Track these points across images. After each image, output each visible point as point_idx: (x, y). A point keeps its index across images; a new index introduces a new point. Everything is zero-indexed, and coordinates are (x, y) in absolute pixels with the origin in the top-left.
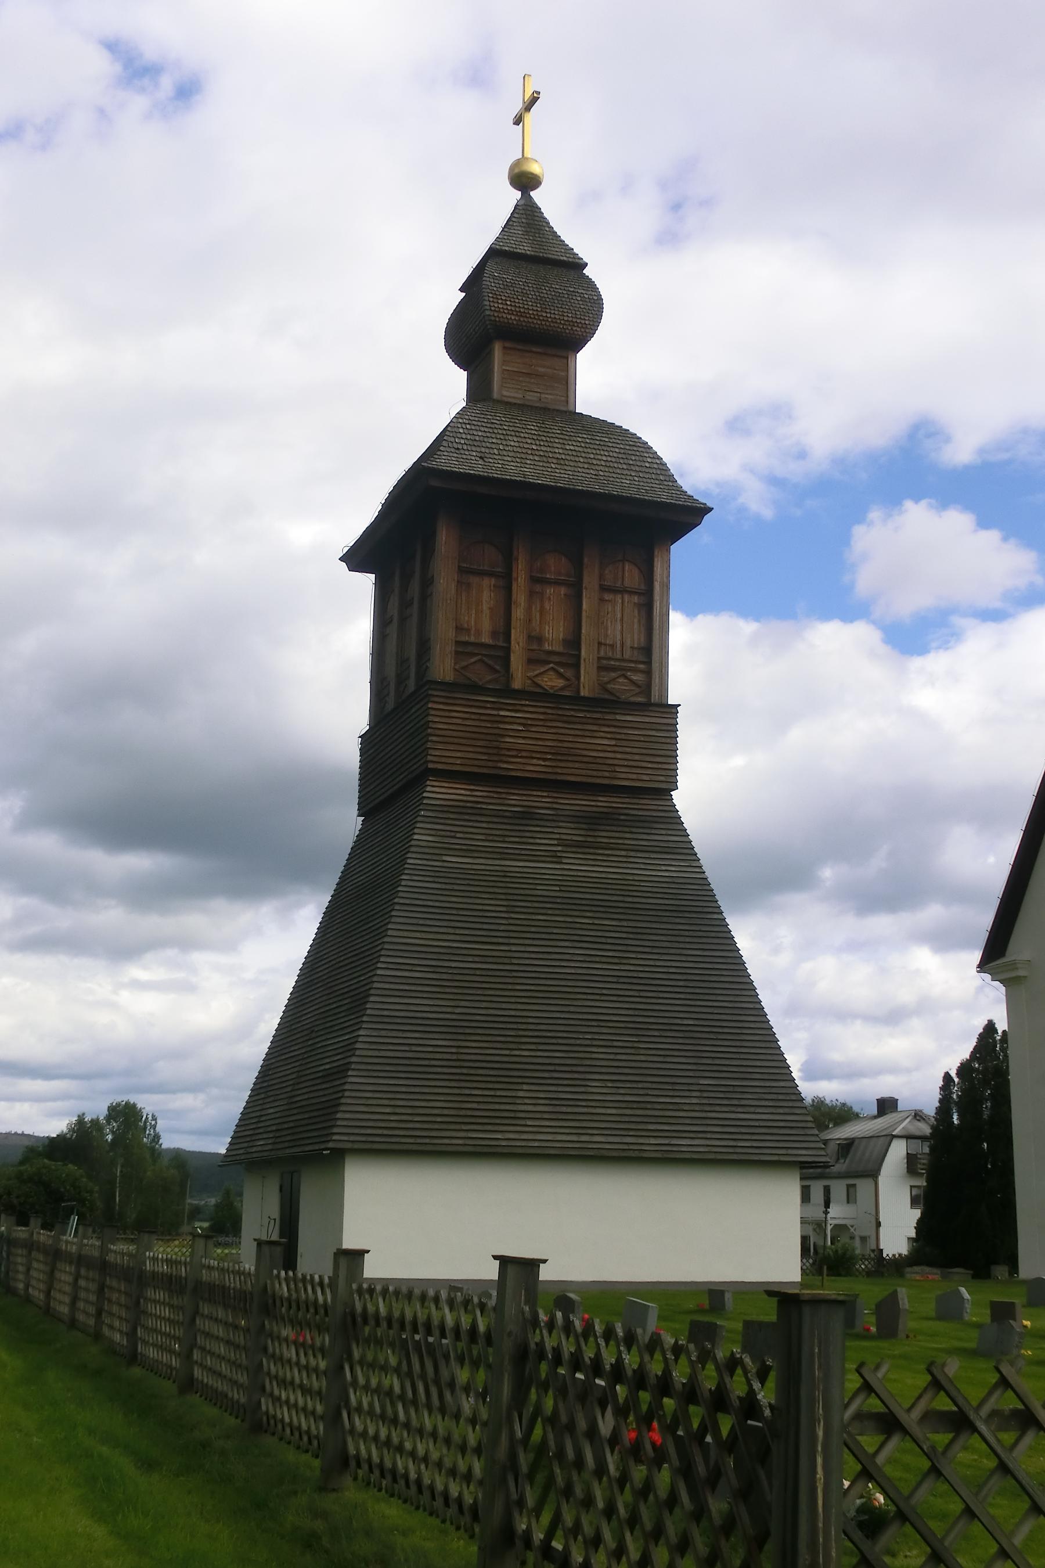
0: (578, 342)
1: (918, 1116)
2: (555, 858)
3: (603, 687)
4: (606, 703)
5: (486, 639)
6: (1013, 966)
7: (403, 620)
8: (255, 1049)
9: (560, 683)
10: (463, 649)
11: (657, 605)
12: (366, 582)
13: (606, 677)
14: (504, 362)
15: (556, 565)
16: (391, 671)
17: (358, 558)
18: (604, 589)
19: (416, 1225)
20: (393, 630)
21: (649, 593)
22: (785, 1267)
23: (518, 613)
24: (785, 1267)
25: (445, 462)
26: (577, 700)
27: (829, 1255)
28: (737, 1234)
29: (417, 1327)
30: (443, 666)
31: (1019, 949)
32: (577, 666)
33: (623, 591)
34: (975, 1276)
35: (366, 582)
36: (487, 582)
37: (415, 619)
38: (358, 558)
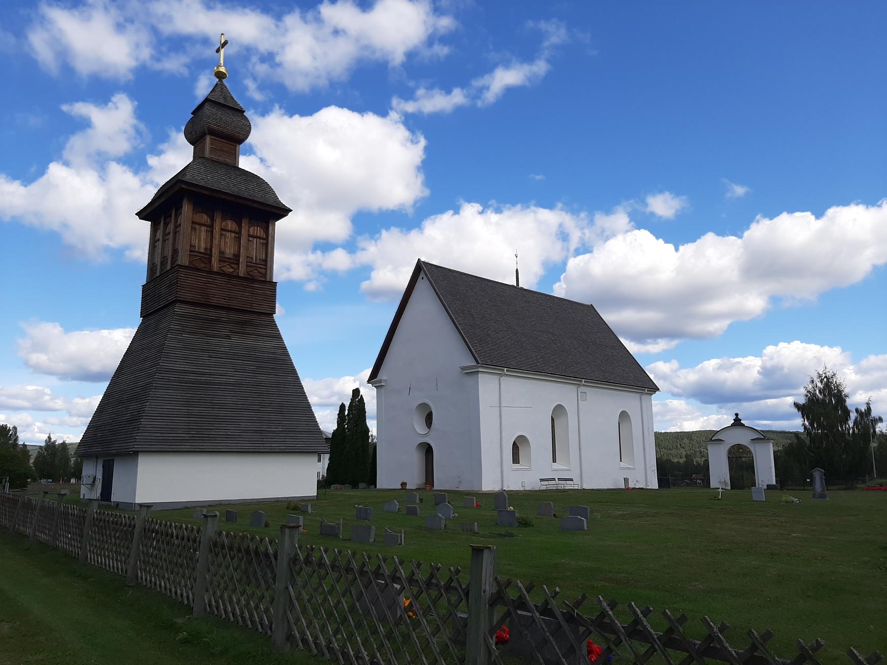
2: (229, 337)
3: (248, 272)
4: (249, 279)
5: (202, 250)
6: (380, 381)
8: (114, 363)
10: (222, 259)
11: (270, 245)
12: (148, 224)
13: (250, 269)
15: (230, 225)
17: (143, 214)
18: (249, 236)
19: (162, 481)
20: (159, 244)
21: (267, 239)
23: (216, 242)
26: (238, 277)
28: (297, 478)
30: (183, 259)
31: (382, 375)
32: (238, 264)
33: (257, 237)
35: (148, 224)
37: (171, 241)
38: (143, 214)
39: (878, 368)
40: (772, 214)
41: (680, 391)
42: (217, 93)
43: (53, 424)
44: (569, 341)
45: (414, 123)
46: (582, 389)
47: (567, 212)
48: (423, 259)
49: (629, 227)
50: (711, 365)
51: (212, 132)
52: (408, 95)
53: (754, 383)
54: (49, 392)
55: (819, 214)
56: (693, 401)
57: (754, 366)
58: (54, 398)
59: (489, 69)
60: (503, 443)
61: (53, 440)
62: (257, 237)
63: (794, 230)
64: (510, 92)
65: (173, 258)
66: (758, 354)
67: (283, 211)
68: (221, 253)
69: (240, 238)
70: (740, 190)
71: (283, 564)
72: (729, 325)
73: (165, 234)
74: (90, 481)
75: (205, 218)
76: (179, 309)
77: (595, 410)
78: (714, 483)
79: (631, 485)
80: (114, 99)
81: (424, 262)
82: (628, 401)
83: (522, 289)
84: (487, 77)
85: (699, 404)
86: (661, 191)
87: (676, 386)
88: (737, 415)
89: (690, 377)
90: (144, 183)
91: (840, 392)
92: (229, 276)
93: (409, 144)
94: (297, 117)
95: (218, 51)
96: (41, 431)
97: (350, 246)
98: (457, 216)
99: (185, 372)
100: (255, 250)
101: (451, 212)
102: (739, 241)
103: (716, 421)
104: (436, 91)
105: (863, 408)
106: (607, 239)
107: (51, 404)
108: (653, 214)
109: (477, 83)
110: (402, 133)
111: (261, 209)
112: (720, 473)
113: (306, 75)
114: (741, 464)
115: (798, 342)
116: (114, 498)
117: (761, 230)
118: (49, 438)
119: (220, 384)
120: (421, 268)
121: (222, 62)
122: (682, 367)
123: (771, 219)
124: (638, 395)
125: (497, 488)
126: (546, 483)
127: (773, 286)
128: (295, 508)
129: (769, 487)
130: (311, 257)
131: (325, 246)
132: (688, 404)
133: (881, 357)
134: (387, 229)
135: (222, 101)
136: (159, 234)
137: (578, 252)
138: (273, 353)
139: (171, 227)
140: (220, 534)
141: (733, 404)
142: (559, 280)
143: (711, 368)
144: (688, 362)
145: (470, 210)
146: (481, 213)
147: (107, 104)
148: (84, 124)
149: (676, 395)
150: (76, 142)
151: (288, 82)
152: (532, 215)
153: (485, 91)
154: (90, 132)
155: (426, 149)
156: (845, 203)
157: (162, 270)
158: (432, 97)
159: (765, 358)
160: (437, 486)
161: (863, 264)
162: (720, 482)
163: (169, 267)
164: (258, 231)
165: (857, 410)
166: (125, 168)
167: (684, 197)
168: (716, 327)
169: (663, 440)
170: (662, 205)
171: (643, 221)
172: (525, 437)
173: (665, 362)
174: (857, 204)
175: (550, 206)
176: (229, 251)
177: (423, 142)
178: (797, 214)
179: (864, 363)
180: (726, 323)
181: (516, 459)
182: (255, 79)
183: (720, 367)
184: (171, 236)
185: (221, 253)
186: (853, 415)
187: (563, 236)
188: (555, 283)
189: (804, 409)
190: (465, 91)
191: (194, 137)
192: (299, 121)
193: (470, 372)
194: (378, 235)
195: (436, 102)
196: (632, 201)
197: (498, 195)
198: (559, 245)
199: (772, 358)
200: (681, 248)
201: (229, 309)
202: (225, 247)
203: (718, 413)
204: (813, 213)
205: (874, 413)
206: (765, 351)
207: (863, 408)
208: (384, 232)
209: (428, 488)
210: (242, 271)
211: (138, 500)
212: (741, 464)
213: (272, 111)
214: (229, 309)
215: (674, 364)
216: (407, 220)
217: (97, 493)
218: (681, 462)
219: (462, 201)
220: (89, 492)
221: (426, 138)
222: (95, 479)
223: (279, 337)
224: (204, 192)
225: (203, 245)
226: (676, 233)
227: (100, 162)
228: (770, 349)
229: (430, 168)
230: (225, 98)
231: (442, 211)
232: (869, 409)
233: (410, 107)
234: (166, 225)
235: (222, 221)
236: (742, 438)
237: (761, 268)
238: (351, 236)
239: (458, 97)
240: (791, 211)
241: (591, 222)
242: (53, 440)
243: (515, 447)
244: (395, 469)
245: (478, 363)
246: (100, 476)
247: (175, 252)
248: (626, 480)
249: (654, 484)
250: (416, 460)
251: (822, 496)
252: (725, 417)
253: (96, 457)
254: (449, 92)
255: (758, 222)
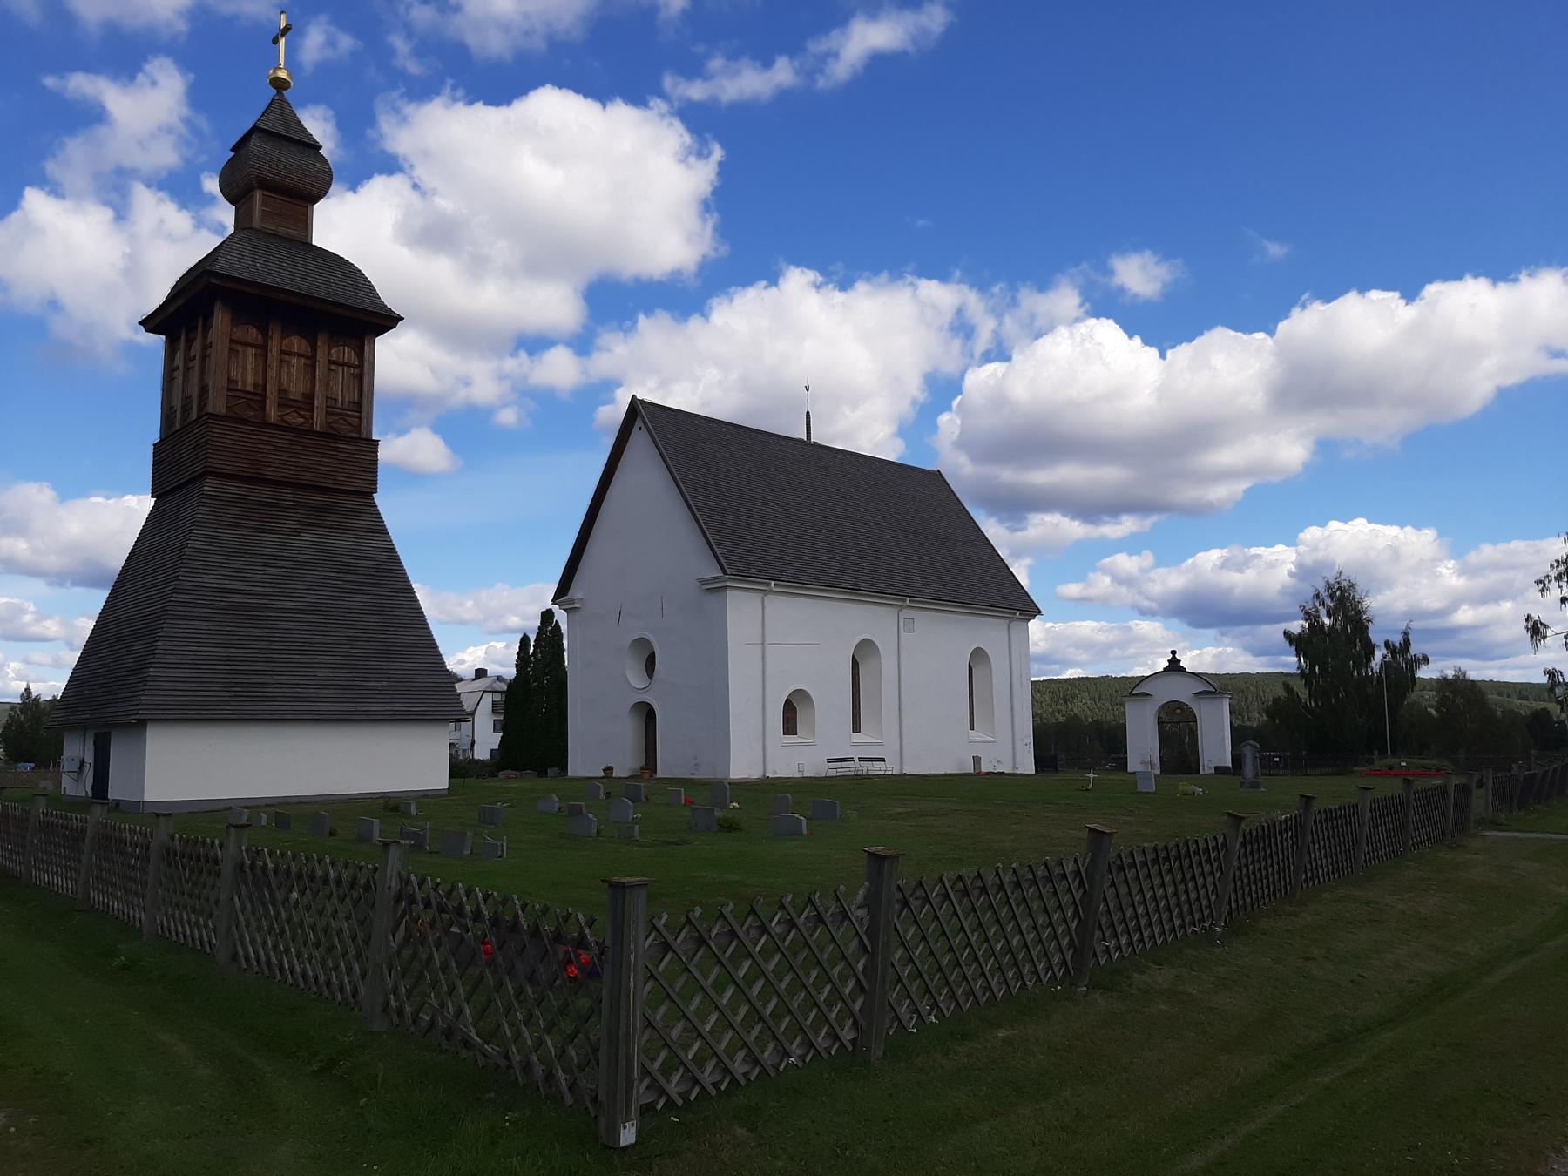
0: (316, 199)
1: (499, 679)
2: (296, 533)
4: (331, 435)
5: (249, 388)
6: (572, 601)
7: (187, 370)
9: (301, 420)
10: (284, 401)
13: (331, 418)
14: (264, 204)
15: (297, 344)
16: (177, 404)
17: (151, 323)
18: (330, 362)
19: (185, 767)
20: (179, 375)
21: (361, 367)
22: (439, 779)
23: (272, 373)
24: (439, 779)
25: (220, 266)
27: (461, 767)
29: (202, 834)
31: (576, 591)
33: (343, 364)
34: (539, 775)
36: (251, 351)
37: (197, 368)
38: (151, 323)
39: (1496, 567)
40: (1329, 295)
41: (1154, 605)
42: (274, 116)
43: (40, 665)
44: (887, 532)
45: (701, 122)
46: (906, 613)
47: (972, 286)
48: (639, 397)
49: (1080, 312)
50: (1210, 558)
51: (264, 185)
52: (693, 69)
53: (1284, 591)
54: (32, 608)
55: (1410, 294)
56: (1175, 622)
57: (1283, 562)
58: (40, 617)
59: (838, 19)
60: (768, 704)
61: (34, 695)
62: (343, 364)
63: (1365, 323)
64: (878, 62)
65: (200, 396)
66: (1291, 542)
67: (387, 320)
68: (282, 392)
69: (314, 367)
70: (1276, 250)
71: (227, 869)
72: (1245, 492)
73: (188, 359)
74: (75, 766)
75: (253, 334)
76: (209, 486)
77: (927, 648)
78: (1133, 765)
79: (984, 770)
80: (147, 67)
81: (642, 401)
82: (987, 632)
83: (816, 445)
84: (835, 33)
85: (1185, 628)
86: (1137, 248)
87: (1148, 598)
88: (1173, 653)
89: (1173, 580)
90: (199, 224)
91: (1359, 613)
92: (296, 430)
93: (692, 159)
94: (479, 106)
95: (276, 41)
96: (20, 677)
97: (582, 344)
98: (774, 290)
99: (221, 591)
100: (340, 386)
101: (763, 283)
102: (1270, 342)
103: (1215, 656)
104: (746, 61)
105: (1397, 640)
106: (1038, 336)
107: (36, 630)
108: (1122, 290)
109: (816, 46)
110: (675, 136)
111: (351, 315)
112: (1143, 746)
113: (505, 27)
114: (1177, 729)
115: (1363, 521)
116: (113, 794)
117: (1308, 322)
118: (28, 690)
119: (282, 610)
120: (636, 408)
121: (282, 60)
122: (1159, 563)
123: (1329, 301)
124: (1005, 623)
125: (756, 774)
126: (838, 765)
127: (1322, 422)
128: (396, 809)
129: (1220, 770)
130: (510, 364)
131: (534, 344)
132: (1167, 628)
133: (1502, 547)
134: (649, 312)
135: (280, 130)
136: (179, 356)
137: (987, 358)
138: (374, 559)
139: (197, 347)
140: (173, 838)
141: (1245, 628)
142: (949, 408)
143: (1209, 566)
144: (1170, 553)
145: (797, 281)
146: (818, 287)
147: (132, 78)
148: (92, 116)
149: (1145, 613)
150: (75, 148)
151: (472, 40)
152: (908, 292)
153: (830, 60)
154: (101, 131)
155: (723, 169)
156: (1455, 275)
157: (184, 419)
158: (737, 73)
159: (1301, 548)
160: (661, 772)
161: (1479, 385)
162: (1143, 763)
163: (194, 416)
164: (347, 354)
165: (1387, 644)
166: (161, 194)
167: (1179, 261)
168: (1218, 493)
169: (1049, 693)
170: (1138, 275)
171: (1104, 303)
172: (803, 691)
173: (1131, 555)
174: (1476, 277)
175: (943, 277)
176: (296, 389)
177: (718, 153)
178: (1375, 295)
179: (1473, 558)
180: (1241, 486)
181: (790, 727)
182: (409, 33)
183: (1225, 565)
184: (197, 363)
185: (282, 392)
186: (1379, 654)
187: (962, 328)
188: (942, 412)
189: (1296, 642)
190: (796, 64)
191: (235, 191)
192: (486, 117)
193: (713, 589)
194: (628, 323)
195: (747, 83)
196: (1085, 266)
197: (852, 253)
198: (957, 344)
199: (1315, 549)
200: (1169, 353)
201: (296, 486)
202: (289, 381)
203: (1217, 643)
204: (1402, 297)
205: (1416, 650)
206: (1301, 535)
207: (1397, 640)
208: (642, 318)
209: (647, 775)
210: (319, 421)
211: (149, 796)
212: (1177, 729)
213: (438, 93)
214: (296, 486)
215: (1147, 559)
216: (683, 297)
217: (86, 787)
218: (1078, 727)
219: (783, 265)
220: (76, 787)
221: (724, 146)
222: (82, 763)
223: (383, 532)
224: (249, 290)
225: (250, 380)
226: (1159, 325)
227: (114, 191)
228: (1312, 533)
229: (725, 205)
230: (286, 124)
231: (746, 281)
232: (1407, 643)
233: (696, 91)
234: (189, 342)
235: (283, 338)
236: (1181, 692)
237: (1304, 388)
238: (585, 327)
239: (783, 73)
240: (1363, 289)
241: (1014, 303)
242: (34, 695)
243: (790, 711)
244: (596, 742)
245: (724, 572)
246: (89, 758)
247: (204, 390)
248: (977, 760)
249: (1028, 766)
250: (629, 731)
251: (1255, 785)
252: (1229, 650)
253: (81, 727)
254: (767, 64)
255: (1304, 307)
